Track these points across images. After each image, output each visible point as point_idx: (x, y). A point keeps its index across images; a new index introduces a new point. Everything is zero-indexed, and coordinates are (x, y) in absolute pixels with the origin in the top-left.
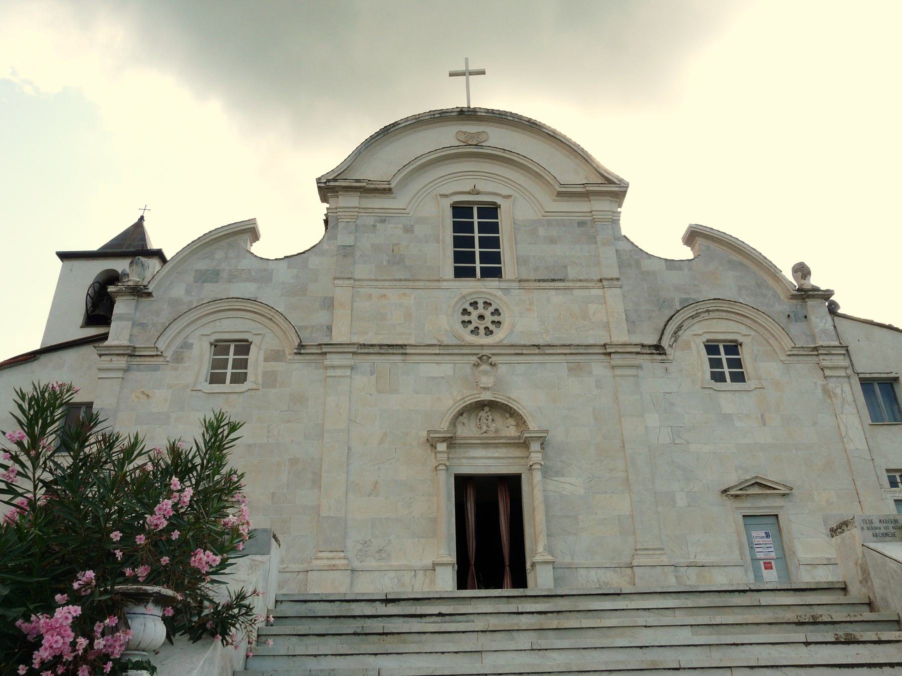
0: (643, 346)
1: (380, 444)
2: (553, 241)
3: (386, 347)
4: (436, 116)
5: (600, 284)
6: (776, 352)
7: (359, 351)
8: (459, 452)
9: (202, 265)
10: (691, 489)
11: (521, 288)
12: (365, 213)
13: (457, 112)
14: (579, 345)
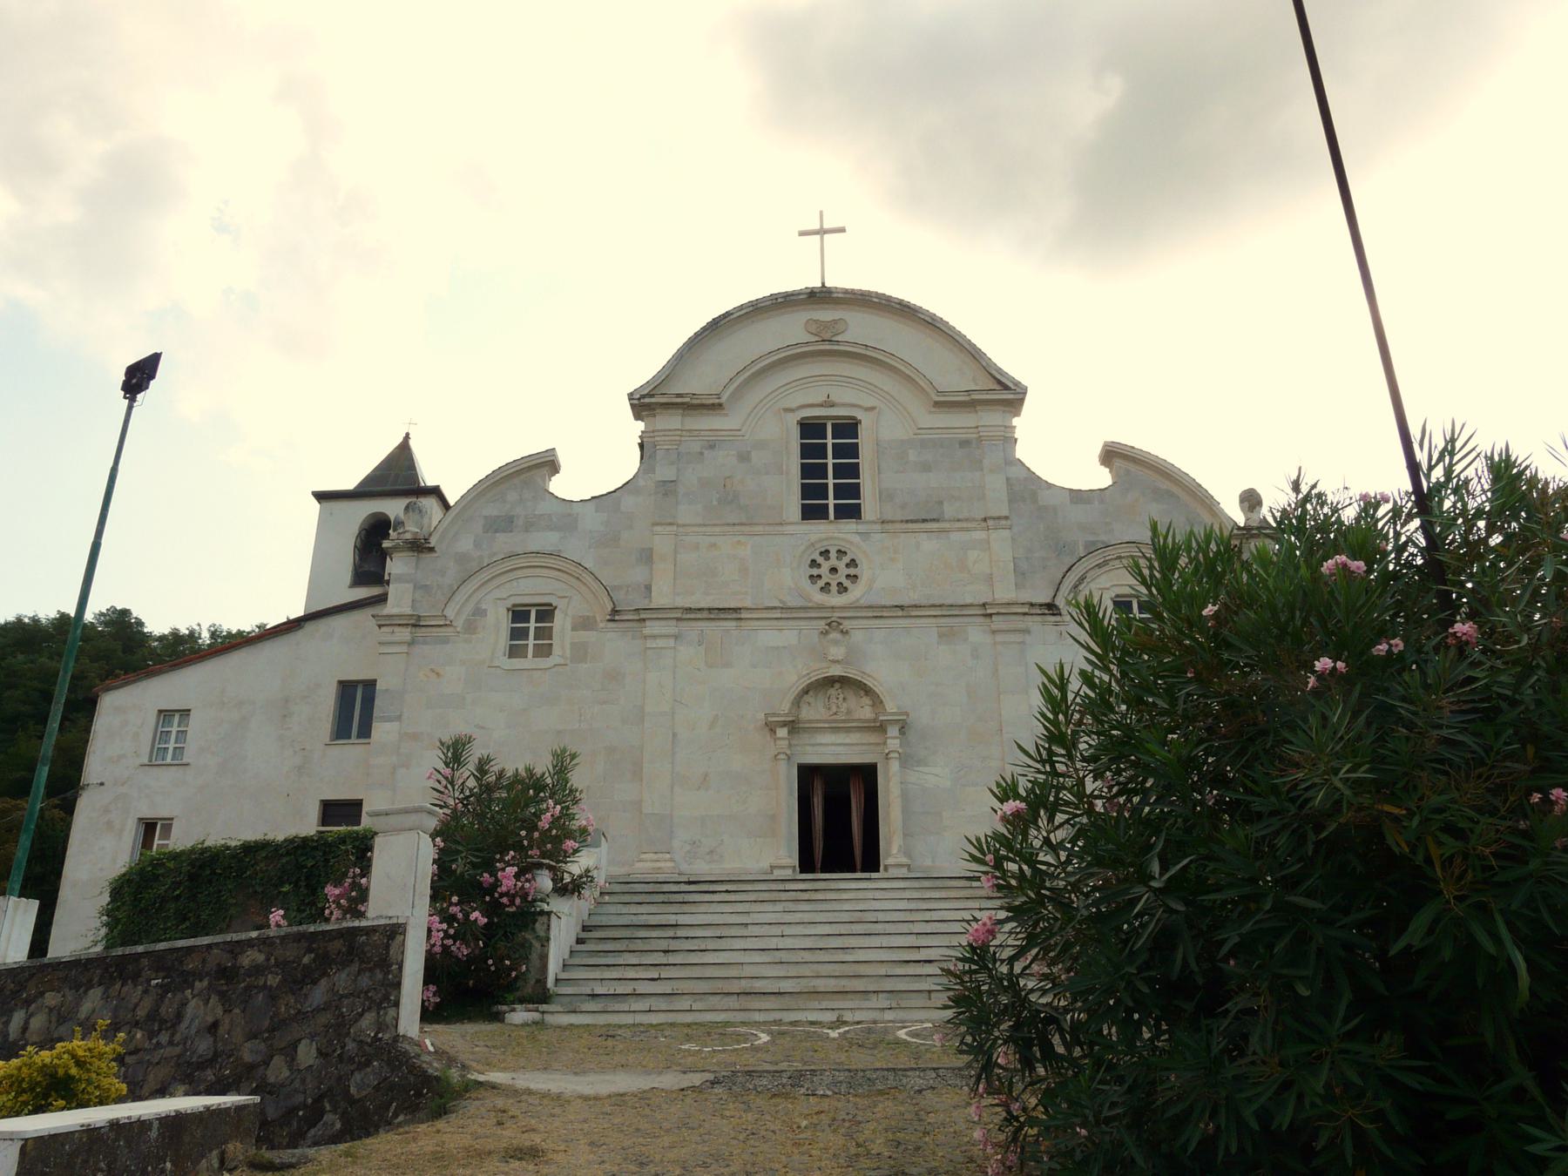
0: (1032, 605)
2: (926, 468)
4: (779, 300)
5: (984, 524)
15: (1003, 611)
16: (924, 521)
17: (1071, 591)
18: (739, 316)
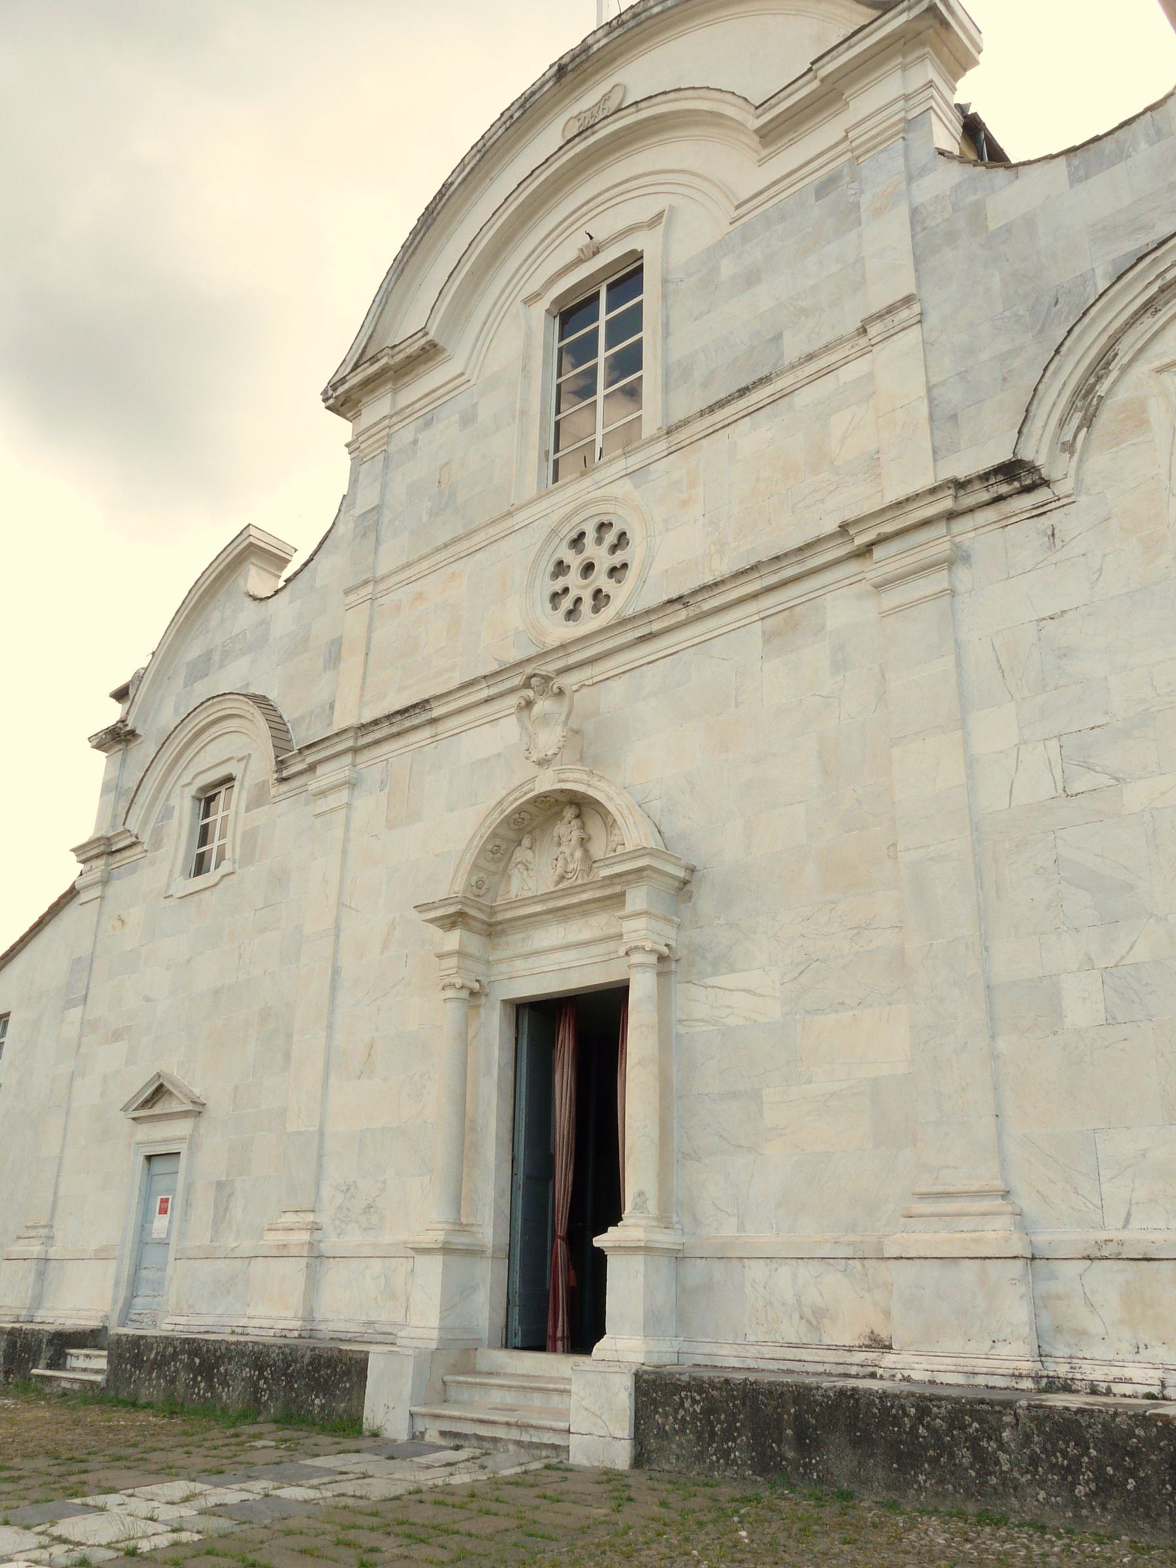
0: (960, 485)
1: (382, 952)
2: (751, 278)
3: (399, 718)
4: (516, 116)
5: (863, 342)
6: (665, 281)
7: (363, 741)
8: (515, 943)
9: (193, 651)
10: (1122, 958)
11: (673, 449)
12: (401, 421)
13: (552, 77)
14: (777, 558)
15: (889, 528)
16: (743, 392)
17: (1072, 407)
18: (464, 180)
